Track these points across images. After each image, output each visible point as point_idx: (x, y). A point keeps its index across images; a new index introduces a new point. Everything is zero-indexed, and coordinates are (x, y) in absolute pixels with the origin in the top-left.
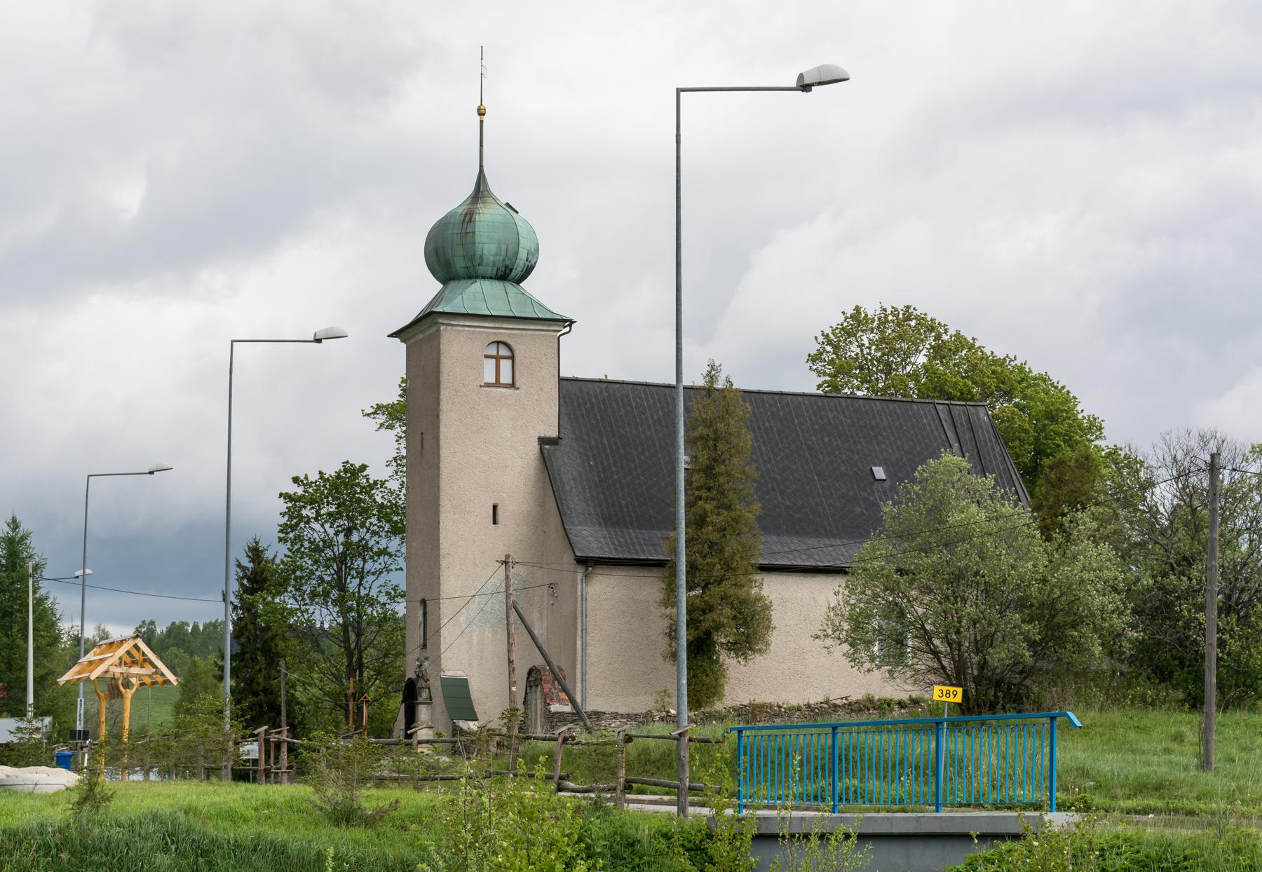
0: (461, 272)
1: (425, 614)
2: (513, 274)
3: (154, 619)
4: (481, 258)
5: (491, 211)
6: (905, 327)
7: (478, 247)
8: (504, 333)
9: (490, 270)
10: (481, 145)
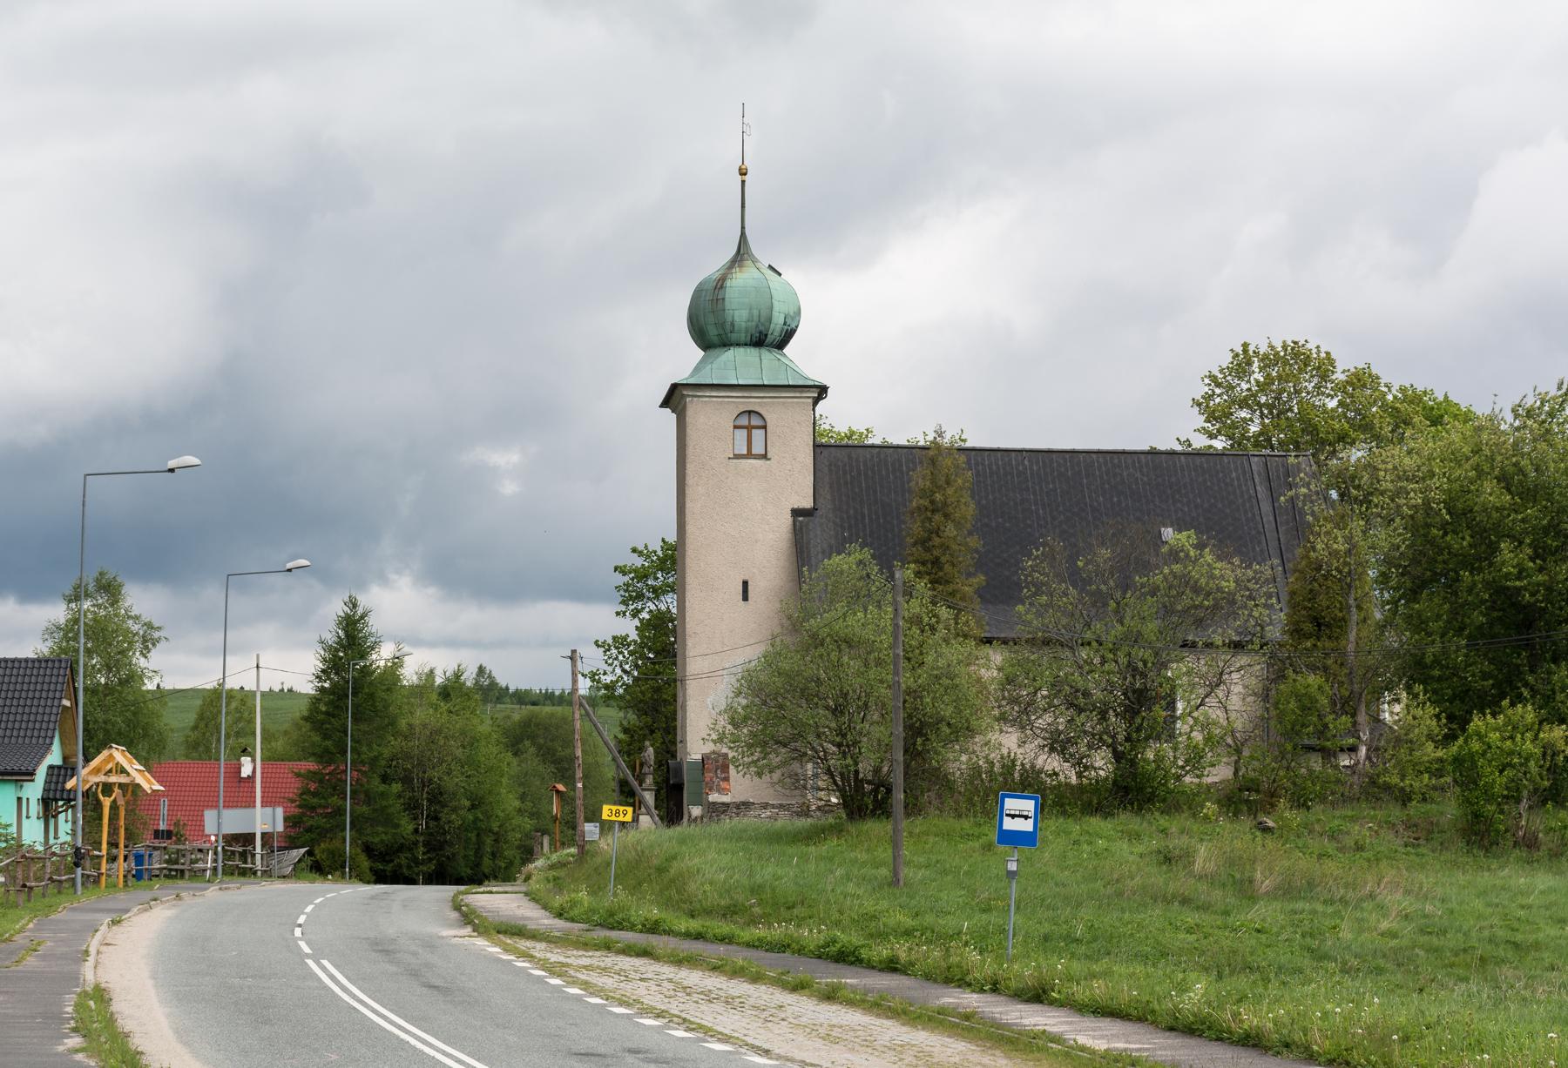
0: (715, 340)
4: (733, 324)
6: (1296, 362)
7: (729, 313)
8: (754, 402)
9: (743, 338)
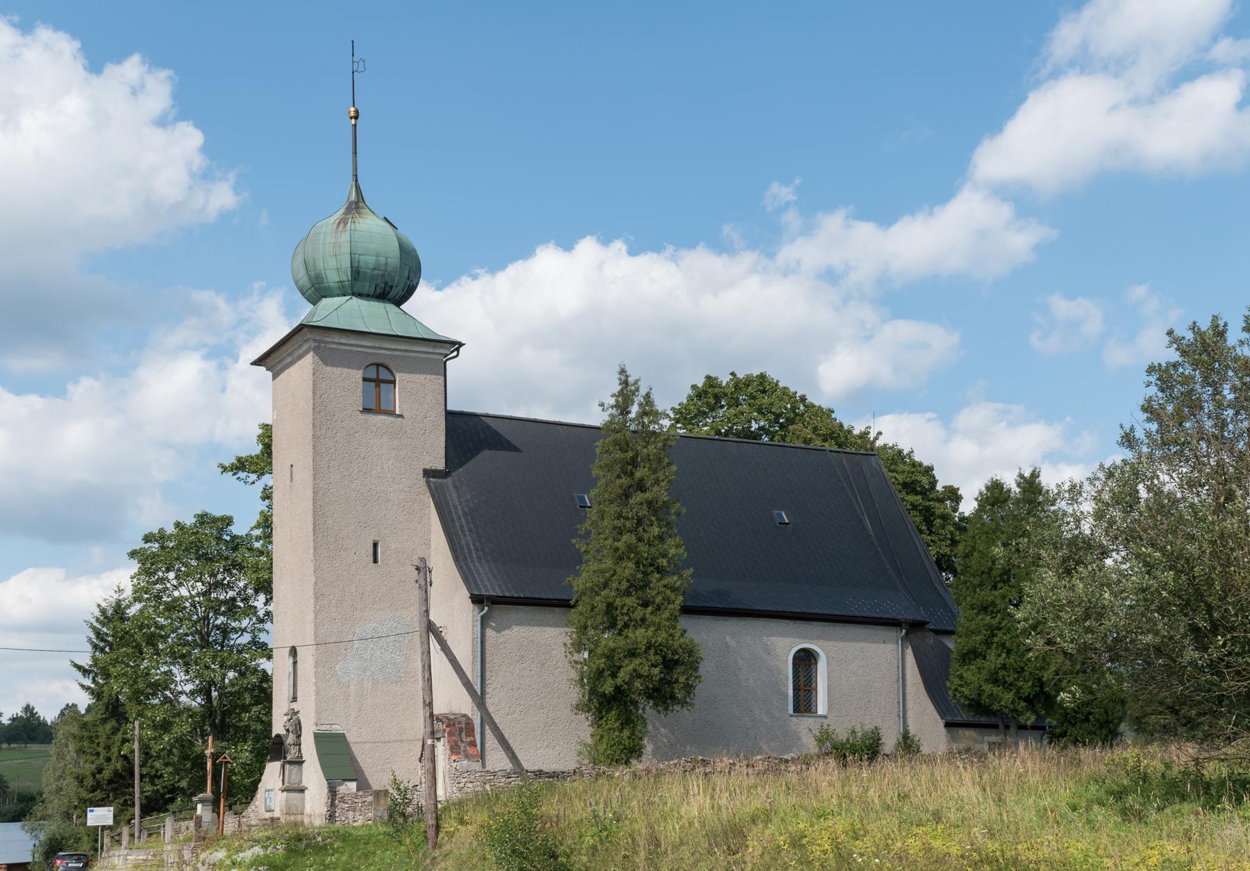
1: (295, 663)
2: (392, 294)
3: (618, 369)
10: (355, 153)
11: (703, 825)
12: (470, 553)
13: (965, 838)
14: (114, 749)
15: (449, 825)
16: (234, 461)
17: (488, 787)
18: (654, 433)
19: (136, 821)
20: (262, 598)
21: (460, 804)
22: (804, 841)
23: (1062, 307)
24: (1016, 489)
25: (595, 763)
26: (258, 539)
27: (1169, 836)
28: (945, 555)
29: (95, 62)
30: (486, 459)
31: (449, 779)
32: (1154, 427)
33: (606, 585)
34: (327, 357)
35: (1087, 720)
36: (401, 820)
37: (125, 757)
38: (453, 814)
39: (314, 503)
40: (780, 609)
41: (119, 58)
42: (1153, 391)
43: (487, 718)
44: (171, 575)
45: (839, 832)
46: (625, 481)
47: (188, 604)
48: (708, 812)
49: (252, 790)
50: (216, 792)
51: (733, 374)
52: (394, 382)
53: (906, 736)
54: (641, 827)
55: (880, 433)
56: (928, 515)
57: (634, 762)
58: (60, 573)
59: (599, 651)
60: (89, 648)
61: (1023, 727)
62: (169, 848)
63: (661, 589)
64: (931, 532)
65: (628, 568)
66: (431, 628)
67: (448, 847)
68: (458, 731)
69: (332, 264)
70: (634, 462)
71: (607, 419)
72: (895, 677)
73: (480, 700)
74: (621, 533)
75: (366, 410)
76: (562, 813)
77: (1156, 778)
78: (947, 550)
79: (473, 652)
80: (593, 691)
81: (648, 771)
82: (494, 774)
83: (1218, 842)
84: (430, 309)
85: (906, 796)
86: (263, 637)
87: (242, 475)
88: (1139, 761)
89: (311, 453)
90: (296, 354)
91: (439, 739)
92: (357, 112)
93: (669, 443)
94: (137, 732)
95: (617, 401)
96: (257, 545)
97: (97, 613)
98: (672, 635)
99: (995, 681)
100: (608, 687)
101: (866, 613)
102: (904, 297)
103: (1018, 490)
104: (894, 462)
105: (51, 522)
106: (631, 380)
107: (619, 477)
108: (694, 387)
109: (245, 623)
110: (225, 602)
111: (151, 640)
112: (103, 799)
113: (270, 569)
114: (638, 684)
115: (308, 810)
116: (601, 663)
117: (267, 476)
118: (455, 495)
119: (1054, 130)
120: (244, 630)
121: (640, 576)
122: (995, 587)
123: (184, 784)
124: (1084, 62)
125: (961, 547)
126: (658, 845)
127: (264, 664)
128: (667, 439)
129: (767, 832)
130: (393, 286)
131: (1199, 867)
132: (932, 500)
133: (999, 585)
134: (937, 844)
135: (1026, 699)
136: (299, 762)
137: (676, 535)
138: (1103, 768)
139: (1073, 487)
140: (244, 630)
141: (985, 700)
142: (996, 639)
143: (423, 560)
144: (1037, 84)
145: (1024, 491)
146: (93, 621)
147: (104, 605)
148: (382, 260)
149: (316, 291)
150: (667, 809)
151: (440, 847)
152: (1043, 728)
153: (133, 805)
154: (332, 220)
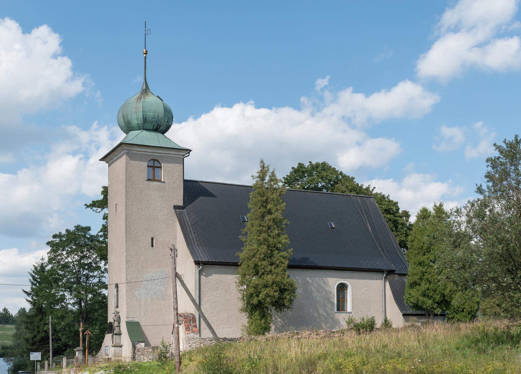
1: (117, 291)
2: (161, 129)
3: (260, 161)
5: (151, 98)
10: (145, 69)
11: (297, 361)
12: (194, 242)
13: (411, 363)
14: (41, 328)
15: (185, 362)
16: (91, 203)
17: (202, 345)
18: (275, 189)
19: (51, 358)
20: (103, 262)
21: (190, 352)
22: (341, 367)
23: (447, 131)
24: (433, 212)
25: (249, 334)
26: (101, 236)
27: (496, 359)
28: (403, 241)
29: (27, 28)
30: (201, 200)
31: (186, 341)
32: (491, 184)
33: (254, 256)
34: (132, 157)
35: (463, 311)
36: (164, 360)
37: (46, 331)
38: (187, 357)
39: (126, 221)
40: (331, 265)
41: (38, 25)
42: (490, 169)
43: (202, 315)
44: (64, 252)
45: (357, 362)
46: (263, 210)
47: (71, 265)
48: (299, 354)
49: (99, 347)
50: (84, 348)
51: (310, 162)
52: (161, 167)
53: (386, 320)
54: (270, 362)
55: (374, 188)
56: (395, 224)
57: (267, 334)
58: (15, 250)
59: (251, 285)
60: (30, 284)
61: (436, 315)
62: (65, 370)
63: (279, 257)
64: (397, 231)
65: (264, 248)
66: (177, 275)
67: (185, 371)
68: (190, 321)
69: (135, 116)
70: (266, 201)
71: (255, 182)
72: (381, 295)
73: (198, 307)
74: (260, 233)
75: (149, 180)
76: (235, 356)
77: (491, 334)
78: (404, 239)
79: (195, 286)
80: (248, 303)
81: (273, 338)
82: (205, 339)
83: (516, 360)
84: (179, 134)
85: (386, 346)
86: (103, 280)
87: (95, 209)
88: (484, 328)
89: (125, 199)
90: (119, 155)
91: (180, 324)
92: (146, 51)
93: (282, 193)
94: (50, 320)
95: (259, 175)
96: (101, 239)
97: (33, 269)
98: (283, 278)
99: (424, 295)
100: (255, 301)
101: (369, 266)
102: (377, 128)
103: (434, 212)
104: (381, 200)
105: (12, 229)
106: (266, 166)
107: (260, 208)
108: (293, 168)
109: (96, 273)
110: (87, 264)
111: (56, 281)
112: (36, 349)
113: (107, 249)
114: (268, 300)
115: (123, 355)
116: (252, 290)
117: (106, 209)
118: (187, 217)
119: (443, 56)
120: (95, 277)
121: (269, 252)
122: (424, 254)
123: (70, 343)
124: (455, 29)
125: (410, 237)
126: (277, 370)
127: (104, 292)
128: (281, 192)
129: (325, 363)
130: (161, 125)
131: (508, 371)
132: (398, 217)
133: (426, 253)
134: (399, 366)
135: (438, 303)
136: (119, 334)
137: (285, 234)
138: (469, 331)
139: (458, 210)
140: (95, 277)
141: (420, 304)
142: (425, 277)
143: (174, 246)
144: (438, 38)
145: (437, 212)
146: (32, 272)
147: (36, 265)
148: (156, 114)
149: (128, 128)
150: (281, 354)
151: (181, 371)
152: (445, 315)
153: (49, 352)
154: (135, 98)
